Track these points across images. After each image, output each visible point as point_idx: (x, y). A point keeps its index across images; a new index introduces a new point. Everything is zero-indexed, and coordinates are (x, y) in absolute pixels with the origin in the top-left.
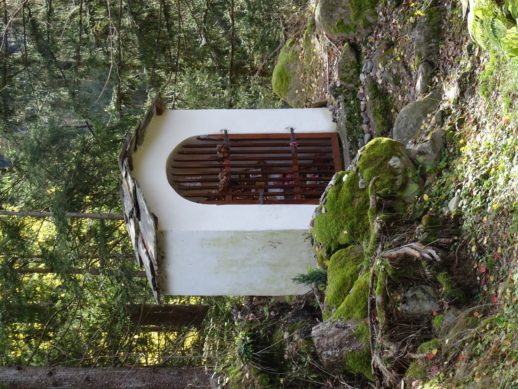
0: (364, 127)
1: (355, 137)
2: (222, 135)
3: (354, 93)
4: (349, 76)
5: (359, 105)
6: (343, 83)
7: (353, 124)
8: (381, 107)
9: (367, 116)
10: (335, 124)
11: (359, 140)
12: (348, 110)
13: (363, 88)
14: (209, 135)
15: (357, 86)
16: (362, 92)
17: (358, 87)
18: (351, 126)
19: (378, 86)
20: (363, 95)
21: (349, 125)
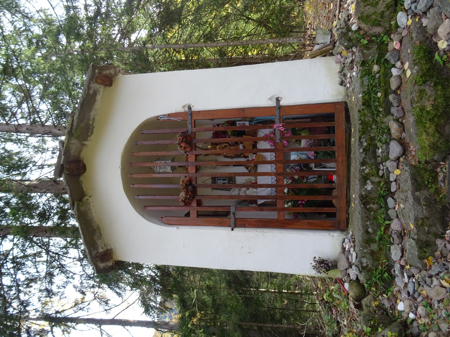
0: (394, 127)
1: (372, 139)
2: (185, 113)
3: (382, 48)
4: (375, 13)
5: (388, 75)
6: (363, 25)
7: (373, 114)
8: (435, 107)
9: (400, 102)
10: (342, 88)
11: (379, 144)
12: (366, 83)
13: (401, 42)
14: (169, 115)
15: (388, 33)
16: (397, 47)
17: (389, 36)
18: (369, 119)
19: (437, 57)
20: (398, 54)
21: (365, 115)
